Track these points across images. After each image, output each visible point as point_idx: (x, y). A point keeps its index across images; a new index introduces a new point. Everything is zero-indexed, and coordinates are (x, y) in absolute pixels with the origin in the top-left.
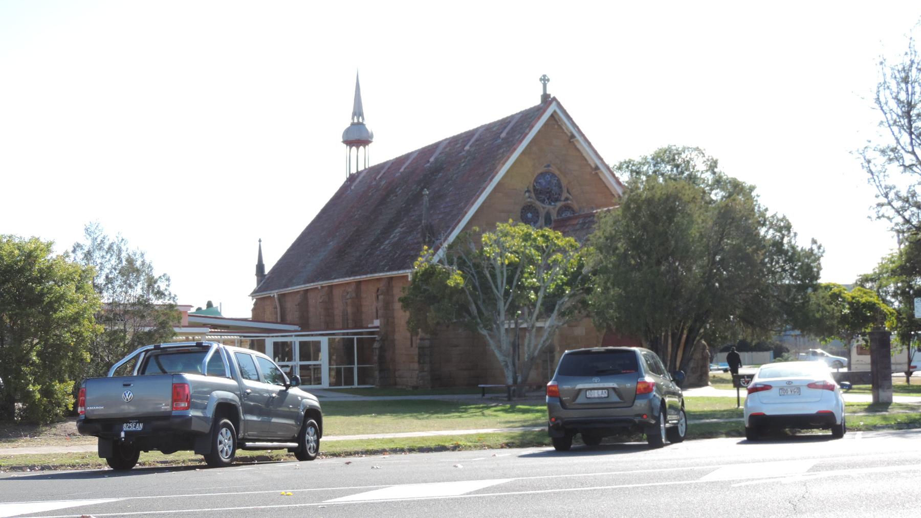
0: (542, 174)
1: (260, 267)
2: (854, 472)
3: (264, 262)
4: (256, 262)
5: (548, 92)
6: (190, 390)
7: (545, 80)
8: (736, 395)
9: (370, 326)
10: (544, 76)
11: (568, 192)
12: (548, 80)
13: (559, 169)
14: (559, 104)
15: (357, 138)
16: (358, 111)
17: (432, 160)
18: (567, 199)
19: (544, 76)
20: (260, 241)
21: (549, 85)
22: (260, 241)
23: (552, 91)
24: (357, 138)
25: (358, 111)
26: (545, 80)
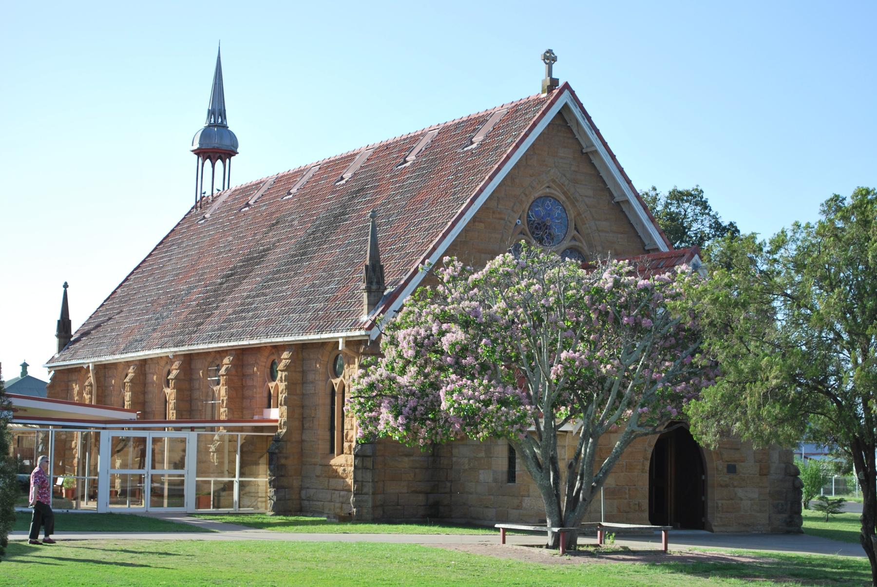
0: (540, 198)
1: (64, 324)
2: (99, 556)
3: (71, 317)
4: (58, 317)
5: (554, 76)
6: (861, 548)
7: (550, 58)
8: (669, 545)
9: (256, 418)
10: (550, 51)
11: (576, 229)
12: (555, 59)
13: (565, 193)
14: (572, 93)
15: (217, 146)
16: (217, 111)
17: (347, 176)
18: (574, 238)
19: (550, 51)
20: (66, 286)
21: (555, 66)
22: (66, 286)
23: (561, 73)
24: (217, 146)
25: (217, 111)
26: (550, 58)
